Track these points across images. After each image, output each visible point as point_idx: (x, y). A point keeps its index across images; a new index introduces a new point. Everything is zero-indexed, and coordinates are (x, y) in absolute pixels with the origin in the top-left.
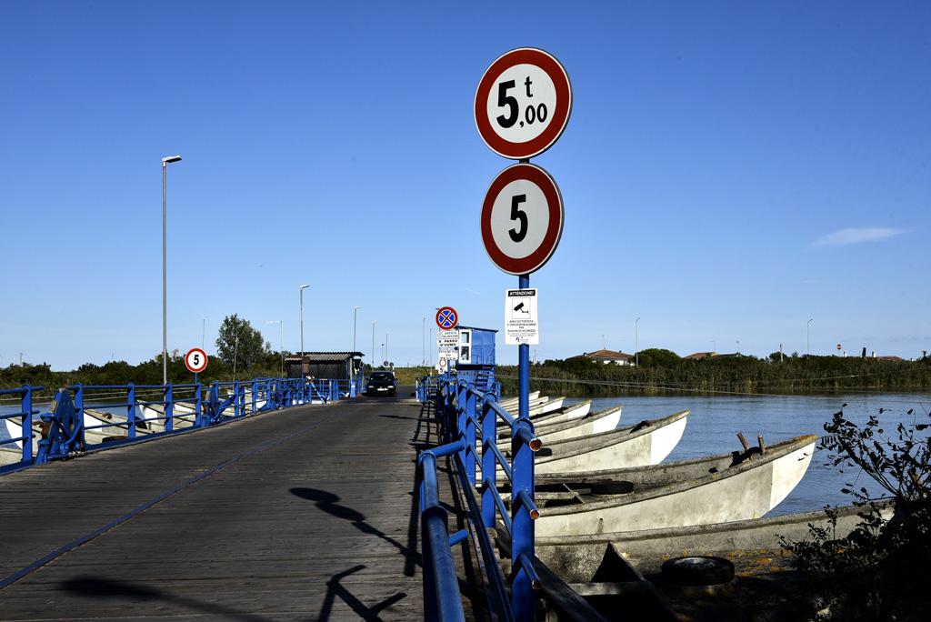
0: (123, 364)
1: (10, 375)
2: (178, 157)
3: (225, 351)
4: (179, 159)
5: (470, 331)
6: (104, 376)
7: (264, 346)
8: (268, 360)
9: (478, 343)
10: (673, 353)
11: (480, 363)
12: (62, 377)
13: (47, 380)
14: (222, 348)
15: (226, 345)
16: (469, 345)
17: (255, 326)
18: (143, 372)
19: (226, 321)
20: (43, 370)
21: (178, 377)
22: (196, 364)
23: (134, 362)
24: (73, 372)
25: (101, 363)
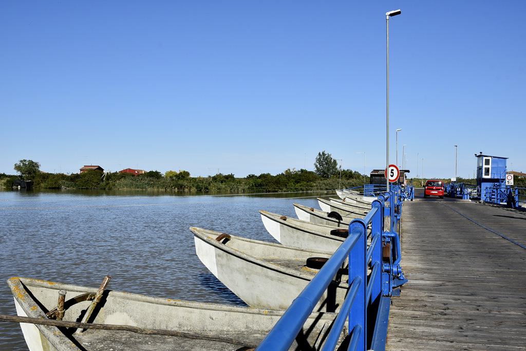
0: (268, 174)
1: (216, 179)
2: (399, 10)
3: (318, 170)
4: (399, 13)
5: (490, 158)
6: (260, 180)
7: (338, 167)
8: (138, 175)
9: (495, 166)
10: (288, 172)
11: (495, 178)
12: (240, 181)
13: (233, 182)
14: (316, 166)
15: (319, 166)
16: (490, 166)
17: (334, 157)
18: (278, 179)
19: (319, 154)
20: (230, 177)
21: (296, 182)
22: (392, 176)
23: (274, 174)
24: (245, 178)
25: (258, 174)
